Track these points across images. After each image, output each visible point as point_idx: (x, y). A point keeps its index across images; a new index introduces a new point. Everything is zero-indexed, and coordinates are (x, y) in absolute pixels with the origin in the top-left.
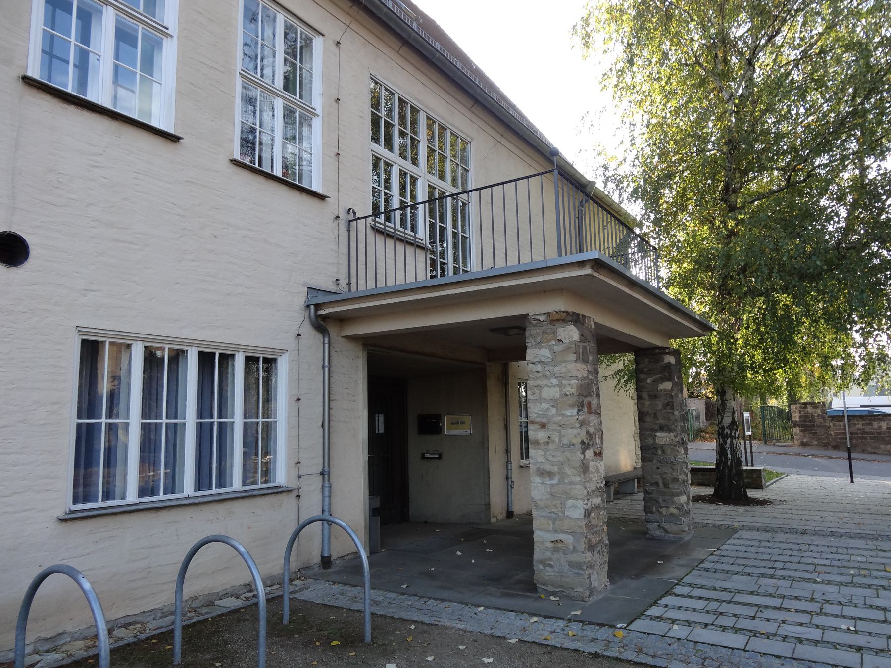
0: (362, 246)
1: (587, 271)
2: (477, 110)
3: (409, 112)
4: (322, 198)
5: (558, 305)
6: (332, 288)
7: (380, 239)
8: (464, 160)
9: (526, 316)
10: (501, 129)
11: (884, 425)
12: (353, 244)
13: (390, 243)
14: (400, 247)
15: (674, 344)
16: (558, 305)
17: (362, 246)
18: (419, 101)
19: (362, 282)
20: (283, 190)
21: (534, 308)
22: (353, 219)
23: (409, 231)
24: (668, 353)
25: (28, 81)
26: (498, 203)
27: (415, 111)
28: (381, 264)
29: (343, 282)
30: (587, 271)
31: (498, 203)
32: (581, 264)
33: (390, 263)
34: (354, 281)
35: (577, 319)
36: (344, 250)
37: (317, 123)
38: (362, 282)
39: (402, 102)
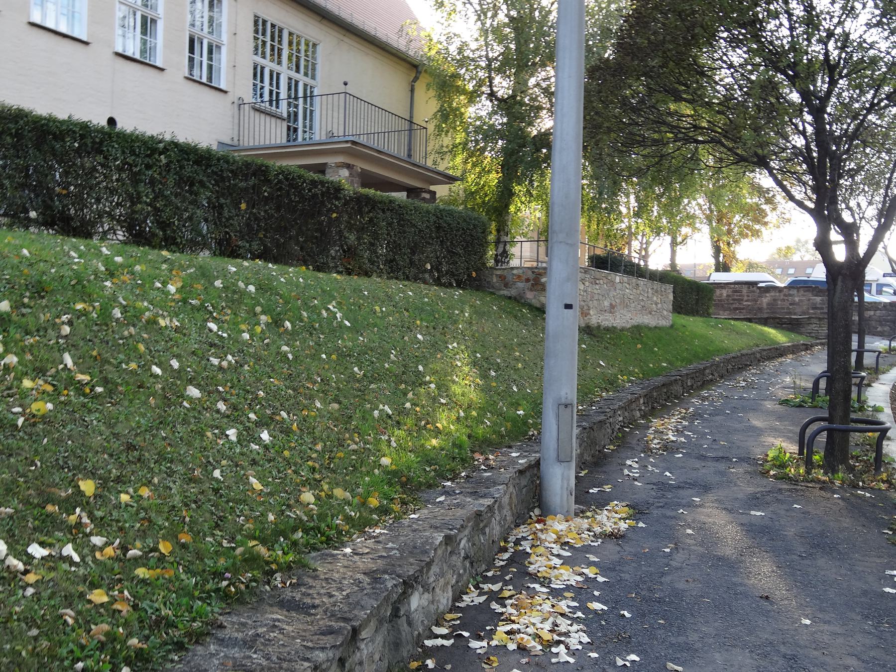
0: (246, 118)
1: (349, 145)
2: (325, 22)
3: (277, 32)
4: (226, 92)
5: (340, 159)
6: (230, 142)
7: (257, 114)
8: (314, 58)
9: (326, 164)
10: (343, 32)
11: (725, 293)
12: (242, 118)
13: (263, 116)
14: (268, 118)
15: (432, 188)
16: (340, 159)
17: (246, 118)
18: (284, 23)
19: (246, 139)
20: (206, 89)
21: (331, 160)
22: (241, 104)
23: (274, 108)
24: (425, 192)
25: (118, 54)
26: (324, 103)
27: (281, 31)
28: (257, 129)
29: (236, 139)
30: (349, 145)
31: (324, 103)
32: (347, 142)
33: (262, 128)
34: (241, 138)
35: (348, 166)
36: (236, 121)
37: (224, 50)
38: (246, 139)
39: (273, 26)
